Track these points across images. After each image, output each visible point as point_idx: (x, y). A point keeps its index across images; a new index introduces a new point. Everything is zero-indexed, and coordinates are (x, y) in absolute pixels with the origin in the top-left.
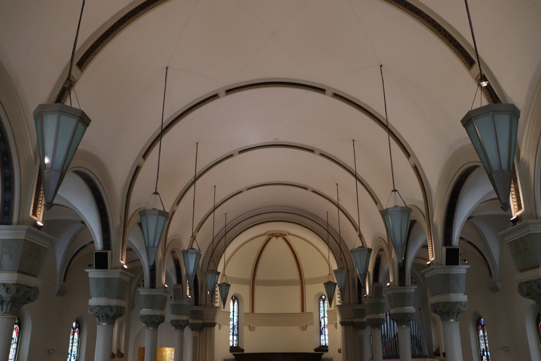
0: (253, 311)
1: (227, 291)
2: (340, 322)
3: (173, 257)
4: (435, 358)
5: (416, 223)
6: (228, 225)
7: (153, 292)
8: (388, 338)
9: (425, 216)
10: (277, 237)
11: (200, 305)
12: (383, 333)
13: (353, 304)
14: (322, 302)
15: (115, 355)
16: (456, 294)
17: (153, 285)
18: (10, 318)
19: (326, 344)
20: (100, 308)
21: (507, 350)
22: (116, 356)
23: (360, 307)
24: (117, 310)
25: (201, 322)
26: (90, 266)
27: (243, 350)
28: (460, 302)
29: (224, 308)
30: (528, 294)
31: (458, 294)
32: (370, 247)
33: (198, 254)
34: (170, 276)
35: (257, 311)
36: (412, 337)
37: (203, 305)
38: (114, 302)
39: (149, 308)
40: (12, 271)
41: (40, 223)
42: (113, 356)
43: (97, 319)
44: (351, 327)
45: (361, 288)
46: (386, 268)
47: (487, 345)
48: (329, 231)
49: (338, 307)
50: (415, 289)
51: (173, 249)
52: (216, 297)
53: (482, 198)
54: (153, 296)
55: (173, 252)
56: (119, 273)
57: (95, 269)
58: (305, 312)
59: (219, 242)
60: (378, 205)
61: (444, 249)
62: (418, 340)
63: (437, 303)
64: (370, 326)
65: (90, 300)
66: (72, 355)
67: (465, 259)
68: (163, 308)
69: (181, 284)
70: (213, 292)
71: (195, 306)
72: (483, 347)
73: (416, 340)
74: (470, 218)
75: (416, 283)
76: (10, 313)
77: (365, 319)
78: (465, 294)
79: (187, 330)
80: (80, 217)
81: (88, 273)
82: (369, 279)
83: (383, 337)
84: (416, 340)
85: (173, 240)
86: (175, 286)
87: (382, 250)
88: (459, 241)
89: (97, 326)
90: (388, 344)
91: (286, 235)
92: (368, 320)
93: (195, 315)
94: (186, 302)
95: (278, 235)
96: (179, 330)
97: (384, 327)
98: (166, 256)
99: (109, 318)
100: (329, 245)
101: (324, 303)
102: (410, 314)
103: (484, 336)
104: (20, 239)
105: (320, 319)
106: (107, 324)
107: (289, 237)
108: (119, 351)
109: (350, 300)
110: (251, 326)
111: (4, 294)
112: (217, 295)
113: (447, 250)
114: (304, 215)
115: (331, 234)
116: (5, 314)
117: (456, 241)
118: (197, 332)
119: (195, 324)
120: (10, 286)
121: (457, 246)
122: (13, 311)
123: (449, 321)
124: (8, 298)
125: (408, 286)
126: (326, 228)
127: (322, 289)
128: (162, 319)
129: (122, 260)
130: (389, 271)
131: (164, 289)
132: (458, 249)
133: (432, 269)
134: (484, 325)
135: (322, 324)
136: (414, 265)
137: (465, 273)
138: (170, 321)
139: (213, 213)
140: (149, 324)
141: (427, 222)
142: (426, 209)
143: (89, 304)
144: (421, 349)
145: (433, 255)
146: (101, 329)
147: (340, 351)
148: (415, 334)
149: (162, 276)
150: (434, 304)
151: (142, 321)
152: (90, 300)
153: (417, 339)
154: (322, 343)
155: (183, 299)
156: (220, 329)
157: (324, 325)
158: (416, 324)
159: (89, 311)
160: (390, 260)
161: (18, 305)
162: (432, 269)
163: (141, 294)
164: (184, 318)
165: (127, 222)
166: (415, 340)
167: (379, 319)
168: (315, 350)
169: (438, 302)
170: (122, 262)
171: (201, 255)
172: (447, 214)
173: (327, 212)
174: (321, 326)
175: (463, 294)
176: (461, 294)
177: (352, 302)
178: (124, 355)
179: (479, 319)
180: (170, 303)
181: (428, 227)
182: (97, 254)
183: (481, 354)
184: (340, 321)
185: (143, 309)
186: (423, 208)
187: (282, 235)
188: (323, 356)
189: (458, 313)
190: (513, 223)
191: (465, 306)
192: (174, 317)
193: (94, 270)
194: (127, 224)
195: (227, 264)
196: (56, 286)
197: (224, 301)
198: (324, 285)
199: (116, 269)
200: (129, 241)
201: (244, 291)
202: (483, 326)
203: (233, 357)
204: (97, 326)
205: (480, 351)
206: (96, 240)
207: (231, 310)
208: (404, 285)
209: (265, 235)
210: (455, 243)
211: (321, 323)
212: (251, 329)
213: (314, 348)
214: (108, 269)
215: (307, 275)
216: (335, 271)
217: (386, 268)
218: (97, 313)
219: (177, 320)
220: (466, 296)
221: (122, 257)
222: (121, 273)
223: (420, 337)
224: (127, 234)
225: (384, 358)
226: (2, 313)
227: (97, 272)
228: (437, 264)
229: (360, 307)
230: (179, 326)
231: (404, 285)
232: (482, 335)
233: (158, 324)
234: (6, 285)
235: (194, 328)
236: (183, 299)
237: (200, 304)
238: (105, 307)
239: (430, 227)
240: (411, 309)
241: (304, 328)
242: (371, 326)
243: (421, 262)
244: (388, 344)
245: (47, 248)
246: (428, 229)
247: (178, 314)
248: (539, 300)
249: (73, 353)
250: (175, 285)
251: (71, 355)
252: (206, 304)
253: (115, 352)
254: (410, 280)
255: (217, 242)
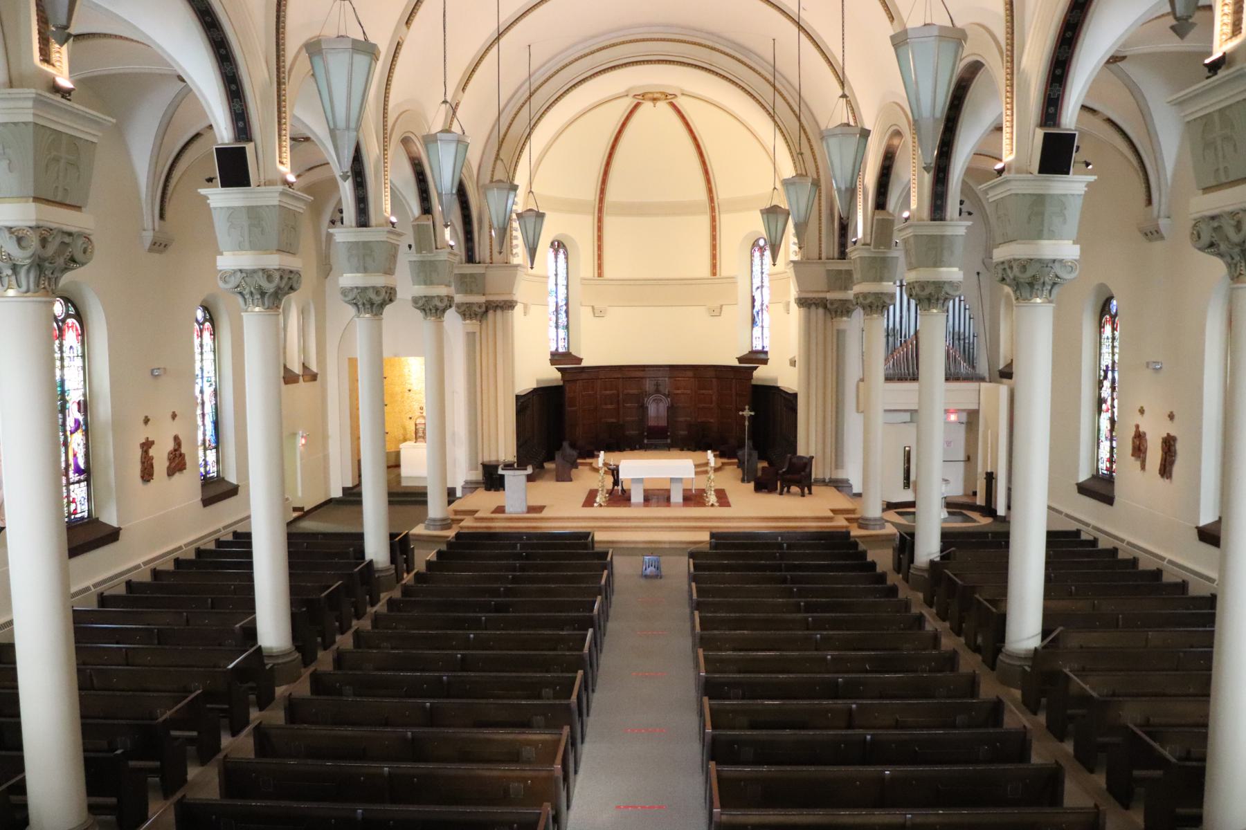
0: (600, 275)
1: (537, 231)
2: (795, 299)
3: (408, 152)
4: (1001, 383)
5: (982, 70)
6: (537, 75)
7: (365, 235)
8: (901, 337)
9: (1004, 51)
10: (654, 100)
11: (479, 263)
12: (891, 326)
13: (828, 259)
14: (757, 254)
15: (298, 376)
16: (1056, 242)
17: (363, 219)
18: (40, 302)
19: (763, 347)
20: (244, 275)
21: (1155, 369)
22: (301, 378)
23: (842, 266)
24: (281, 278)
25: (480, 299)
26: (210, 180)
27: (580, 360)
28: (1061, 261)
29: (532, 268)
30: (1212, 245)
31: (1060, 242)
32: (867, 127)
33: (462, 144)
34: (404, 198)
35: (608, 272)
36: (956, 337)
37: (484, 263)
38: (273, 261)
39: (358, 272)
40: (21, 197)
41: (65, 82)
42: (289, 378)
43: (240, 300)
44: (821, 311)
45: (844, 228)
46: (905, 180)
47: (1116, 357)
48: (777, 84)
49: (792, 264)
50: (968, 227)
51: (407, 135)
52: (515, 242)
53: (1148, 10)
54: (365, 243)
55: (405, 141)
56: (277, 195)
57: (222, 186)
58: (718, 276)
59: (516, 115)
60: (895, 22)
61: (1040, 134)
62: (969, 343)
63: (1010, 261)
64: (862, 311)
65: (219, 258)
66: (205, 379)
67: (1088, 161)
68: (390, 271)
69: (430, 216)
70: (504, 231)
71: (467, 265)
72: (1106, 360)
73: (964, 343)
74: (1114, 60)
75: (970, 214)
76: (37, 292)
77: (850, 294)
78: (1075, 243)
79: (451, 316)
80: (170, 66)
81: (206, 198)
82: (865, 200)
83: (891, 333)
84: (964, 343)
85: (404, 112)
86: (417, 219)
87: (898, 133)
88: (1079, 115)
89: (242, 314)
90: (901, 349)
91: (675, 96)
92: (857, 296)
93: (467, 284)
94: (443, 256)
95: (656, 96)
96: (433, 318)
97: (894, 311)
98: (390, 153)
99: (267, 296)
100: (776, 118)
101: (762, 255)
102: (951, 283)
103: (1113, 339)
104: (24, 123)
105: (752, 292)
106: (263, 310)
107: (681, 102)
108: (305, 367)
109: (820, 251)
110: (595, 307)
111: (11, 247)
112: (516, 238)
113: (1047, 137)
114: (717, 46)
115: (782, 95)
116: (28, 294)
117: (1070, 118)
118: (474, 321)
119: (469, 305)
120: (25, 232)
121: (1073, 128)
122: (44, 288)
123: (1032, 301)
124: (27, 258)
125: (952, 220)
126: (771, 79)
127: (756, 225)
128: (390, 295)
129: (281, 162)
130: (910, 188)
131: (390, 227)
132: (1074, 135)
133: (1007, 181)
134: (1116, 315)
135: (757, 304)
136: (970, 171)
137: (1083, 193)
138: (410, 298)
139: (496, 46)
140: (360, 306)
141: (1007, 68)
142: (1007, 33)
143: (218, 268)
144: (973, 363)
145: (1012, 150)
146: (253, 320)
147: (793, 363)
148: (962, 330)
149: (382, 198)
150: (1003, 263)
151: (346, 302)
152: (219, 258)
153: (967, 341)
154: (754, 346)
155: (437, 248)
156: (525, 314)
157: (762, 305)
158: (967, 307)
159: (221, 284)
160: (914, 159)
161: (52, 273)
162: (1007, 181)
163: (338, 241)
164: (442, 291)
165: (284, 73)
166: (962, 342)
167: (882, 293)
168: (741, 360)
169: (1012, 257)
170: (282, 168)
171: (467, 147)
172: (1055, 48)
173: (774, 40)
174: (753, 307)
175: (1071, 242)
176: (1066, 242)
177: (824, 256)
178: (319, 376)
179: (1108, 301)
180: (406, 259)
181: (1007, 80)
182: (222, 153)
183: (1100, 376)
184: (797, 296)
185: (345, 275)
186: (1001, 32)
187: (668, 98)
188: (756, 374)
189: (1055, 284)
190: (1210, 71)
191: (1072, 269)
192: (421, 290)
193: (220, 190)
194: (284, 78)
195: (537, 169)
196: (144, 230)
197: (532, 252)
198: (760, 215)
199: (269, 185)
200: (294, 116)
201: (580, 231)
202: (1114, 317)
203: (559, 375)
204: (242, 314)
205: (1100, 369)
206: (215, 120)
207: (551, 273)
208: (942, 219)
209: (627, 95)
210: (1068, 120)
211: (753, 300)
212: (597, 313)
213: (738, 356)
214: (250, 186)
215: (723, 193)
216: (787, 183)
217: (905, 180)
218: (238, 286)
219: (425, 297)
220: (1077, 247)
221: (280, 157)
222: (283, 193)
223: (974, 336)
224: (287, 101)
225: (888, 379)
226: (19, 292)
227: (225, 193)
228: (1019, 171)
229: (842, 266)
230: (432, 308)
231: (942, 219)
232: (1110, 336)
233: (382, 305)
234: (13, 230)
235: (467, 312)
236: (437, 248)
237: (477, 260)
238: (254, 271)
239: (1012, 79)
240: (952, 273)
241: (716, 312)
242: (864, 309)
243: (985, 164)
244: (901, 349)
245: (92, 142)
246: (1007, 86)
247: (428, 282)
248: (1233, 259)
249: (205, 374)
250: (418, 218)
251: (202, 378)
252: (491, 259)
253: (297, 368)
254: (958, 206)
255: (509, 120)
